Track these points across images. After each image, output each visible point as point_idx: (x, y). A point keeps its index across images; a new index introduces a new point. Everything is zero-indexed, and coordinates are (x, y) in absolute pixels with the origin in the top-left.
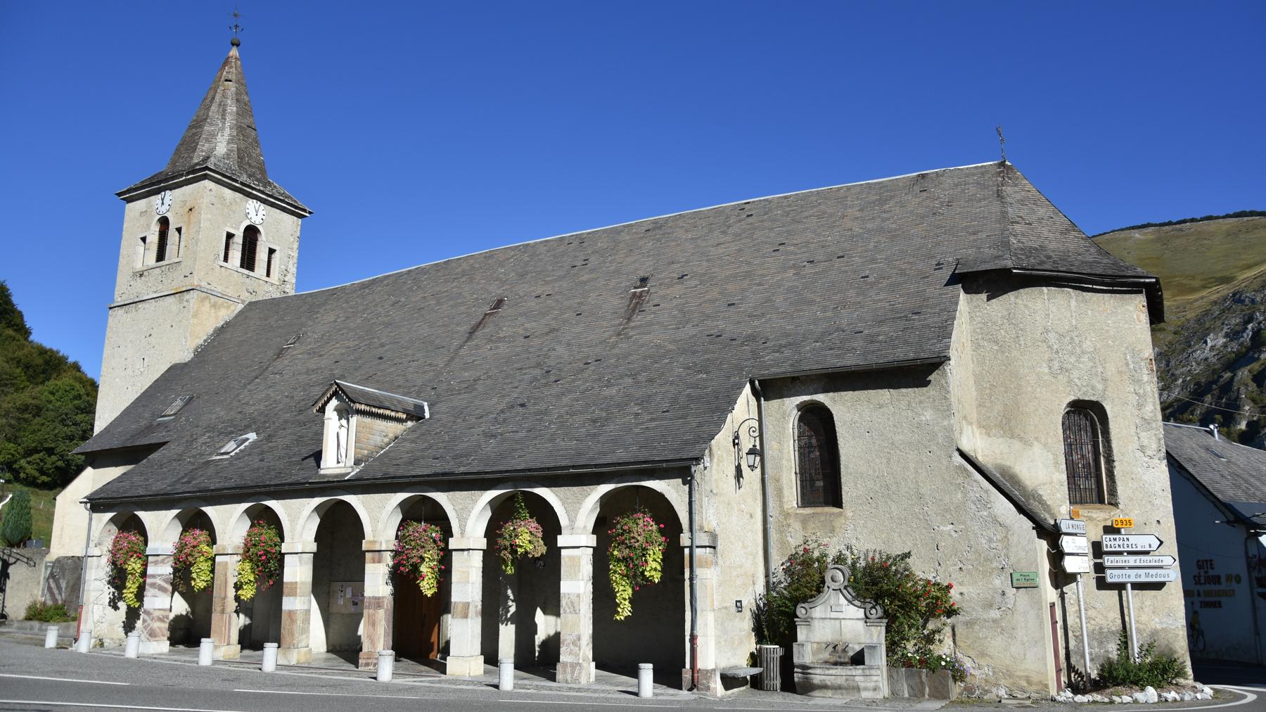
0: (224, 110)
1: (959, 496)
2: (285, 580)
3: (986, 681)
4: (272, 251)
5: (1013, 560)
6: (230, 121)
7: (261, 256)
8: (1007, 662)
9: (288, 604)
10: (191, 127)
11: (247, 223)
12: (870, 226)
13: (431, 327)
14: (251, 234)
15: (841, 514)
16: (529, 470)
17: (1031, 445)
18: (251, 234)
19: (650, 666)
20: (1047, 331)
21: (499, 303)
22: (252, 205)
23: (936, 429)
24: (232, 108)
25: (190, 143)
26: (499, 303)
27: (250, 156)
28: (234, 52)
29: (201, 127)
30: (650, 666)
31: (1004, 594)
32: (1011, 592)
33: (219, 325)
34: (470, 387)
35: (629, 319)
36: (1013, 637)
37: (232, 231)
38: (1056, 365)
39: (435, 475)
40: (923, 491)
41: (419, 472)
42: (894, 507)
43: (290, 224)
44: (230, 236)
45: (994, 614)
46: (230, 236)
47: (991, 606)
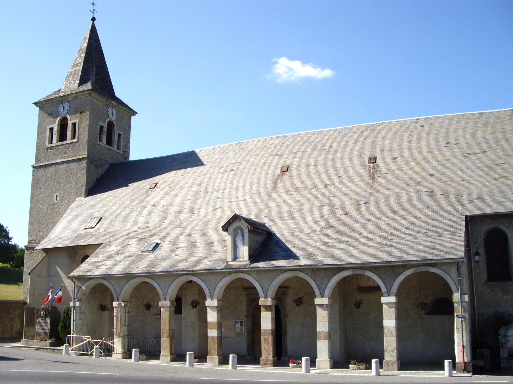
4: (119, 135)
11: (108, 120)
37: (102, 124)
46: (102, 127)
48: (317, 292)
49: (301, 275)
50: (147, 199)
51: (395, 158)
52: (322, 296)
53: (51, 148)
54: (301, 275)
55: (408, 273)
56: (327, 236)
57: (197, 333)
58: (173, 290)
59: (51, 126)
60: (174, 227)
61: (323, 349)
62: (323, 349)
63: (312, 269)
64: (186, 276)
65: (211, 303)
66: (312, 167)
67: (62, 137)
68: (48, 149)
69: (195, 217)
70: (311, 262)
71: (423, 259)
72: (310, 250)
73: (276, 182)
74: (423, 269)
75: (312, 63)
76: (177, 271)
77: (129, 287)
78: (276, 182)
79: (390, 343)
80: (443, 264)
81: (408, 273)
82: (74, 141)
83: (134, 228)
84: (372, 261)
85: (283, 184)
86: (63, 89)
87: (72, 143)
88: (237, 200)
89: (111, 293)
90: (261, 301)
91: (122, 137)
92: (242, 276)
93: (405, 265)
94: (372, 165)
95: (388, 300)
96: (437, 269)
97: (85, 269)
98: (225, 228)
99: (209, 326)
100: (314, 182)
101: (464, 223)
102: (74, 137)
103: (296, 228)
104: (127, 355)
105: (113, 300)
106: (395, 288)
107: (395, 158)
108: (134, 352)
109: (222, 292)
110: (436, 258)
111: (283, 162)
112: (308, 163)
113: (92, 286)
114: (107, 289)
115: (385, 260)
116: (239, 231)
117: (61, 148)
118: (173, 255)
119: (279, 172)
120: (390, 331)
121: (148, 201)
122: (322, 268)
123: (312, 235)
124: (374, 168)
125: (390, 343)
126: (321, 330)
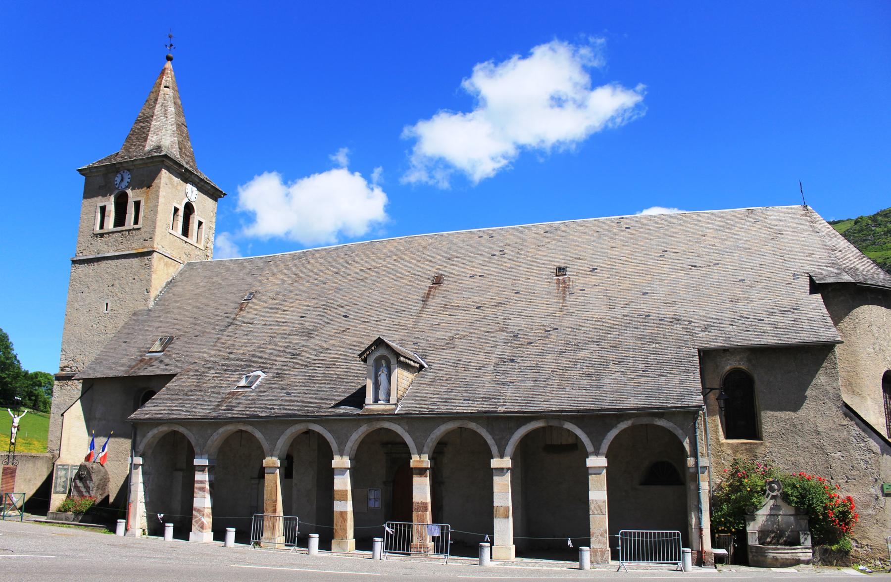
0: (166, 111)
1: (845, 433)
2: (335, 488)
3: (867, 555)
4: (200, 223)
5: (883, 476)
6: (172, 118)
7: (194, 226)
8: (881, 542)
9: (338, 506)
10: (138, 122)
11: (186, 200)
12: (728, 243)
13: (382, 293)
14: (189, 209)
15: (762, 444)
16: (562, 411)
17: (866, 399)
18: (189, 209)
19: (172, 525)
20: (872, 325)
21: (438, 281)
22: (189, 187)
23: (828, 388)
24: (172, 109)
25: (141, 132)
26: (438, 281)
27: (185, 148)
28: (169, 65)
29: (148, 122)
30: (172, 525)
31: (877, 499)
32: (881, 498)
33: (169, 280)
34: (450, 343)
35: (564, 299)
36: (884, 526)
37: (178, 207)
38: (877, 347)
39: (479, 412)
40: (820, 429)
41: (533, 409)
42: (799, 439)
43: (209, 203)
44: (176, 210)
45: (870, 511)
46: (176, 210)
47: (869, 506)
48: (494, 449)
49: (473, 426)
50: (243, 314)
51: (593, 270)
52: (597, 453)
53: (102, 235)
54: (473, 426)
55: (623, 426)
56: (505, 373)
57: (315, 506)
58: (283, 442)
59: (102, 204)
60: (280, 353)
61: (504, 529)
62: (504, 529)
63: (488, 417)
64: (303, 424)
65: (341, 462)
66: (477, 278)
67: (120, 220)
68: (96, 235)
69: (312, 342)
70: (486, 407)
71: (645, 406)
72: (482, 391)
73: (426, 299)
74: (645, 421)
75: (225, 233)
76: (291, 417)
77: (218, 436)
78: (426, 299)
79: (599, 522)
80: (673, 413)
81: (623, 426)
82: (136, 227)
83: (223, 354)
84: (574, 408)
85: (436, 302)
86: (122, 152)
87: (134, 229)
88: (372, 319)
89: (189, 443)
90: (415, 461)
91: (203, 225)
92: (387, 425)
93: (621, 415)
94: (561, 278)
95: (598, 462)
96: (665, 421)
97: (150, 410)
98: (364, 357)
99: (336, 496)
100: (480, 298)
101: (696, 359)
102: (136, 222)
103: (459, 360)
104: (156, 530)
105: (192, 455)
106: (605, 446)
107: (593, 270)
108: (231, 533)
109: (355, 448)
110: (665, 405)
111: (433, 271)
112: (472, 273)
113: (162, 435)
114: (183, 436)
115: (592, 407)
116: (383, 362)
117: (117, 235)
118: (283, 393)
119: (430, 284)
120: (599, 507)
121: (243, 317)
122: (502, 417)
123: (482, 371)
124: (564, 282)
125: (599, 522)
126: (499, 505)
